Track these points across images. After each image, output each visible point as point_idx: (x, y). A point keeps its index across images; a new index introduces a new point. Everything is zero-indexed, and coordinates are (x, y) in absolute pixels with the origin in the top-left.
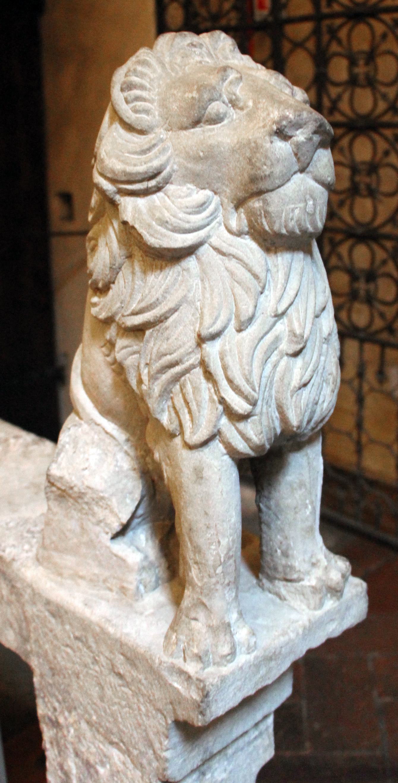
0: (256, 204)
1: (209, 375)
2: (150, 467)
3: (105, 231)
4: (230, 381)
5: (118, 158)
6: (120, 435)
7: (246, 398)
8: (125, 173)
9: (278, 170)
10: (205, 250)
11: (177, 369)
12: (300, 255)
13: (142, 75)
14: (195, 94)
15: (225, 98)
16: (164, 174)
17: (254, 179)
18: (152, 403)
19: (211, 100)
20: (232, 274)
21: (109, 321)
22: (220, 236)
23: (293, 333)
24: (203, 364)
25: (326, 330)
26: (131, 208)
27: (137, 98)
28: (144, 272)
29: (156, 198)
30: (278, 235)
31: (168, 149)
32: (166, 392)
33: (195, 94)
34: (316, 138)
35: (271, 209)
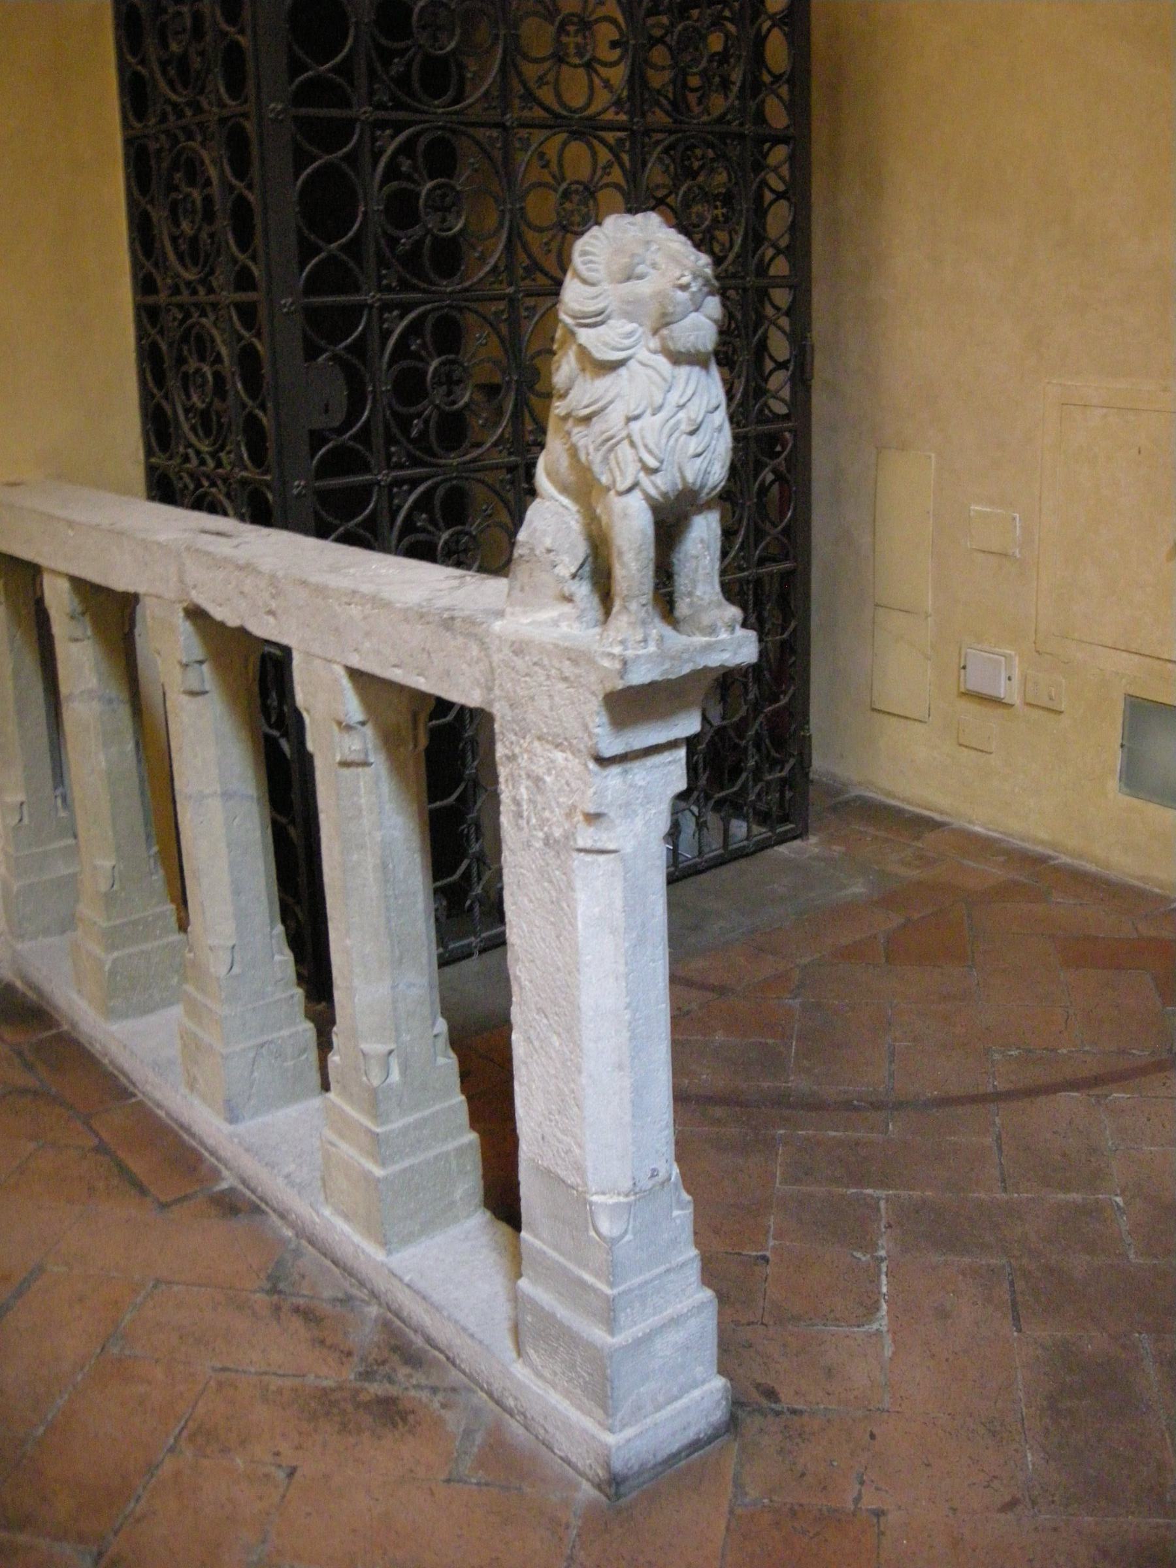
0: (665, 332)
1: (633, 444)
2: (595, 533)
3: (566, 354)
4: (646, 446)
6: (573, 507)
7: (655, 457)
9: (679, 309)
10: (632, 363)
11: (614, 441)
12: (697, 369)
13: (592, 245)
16: (607, 313)
17: (664, 315)
18: (597, 468)
20: (649, 377)
21: (565, 418)
22: (643, 354)
23: (689, 419)
24: (629, 436)
25: (717, 423)
26: (585, 336)
27: (591, 262)
28: (592, 379)
29: (601, 329)
30: (680, 353)
31: (610, 295)
32: (605, 460)
34: (705, 289)
35: (675, 335)
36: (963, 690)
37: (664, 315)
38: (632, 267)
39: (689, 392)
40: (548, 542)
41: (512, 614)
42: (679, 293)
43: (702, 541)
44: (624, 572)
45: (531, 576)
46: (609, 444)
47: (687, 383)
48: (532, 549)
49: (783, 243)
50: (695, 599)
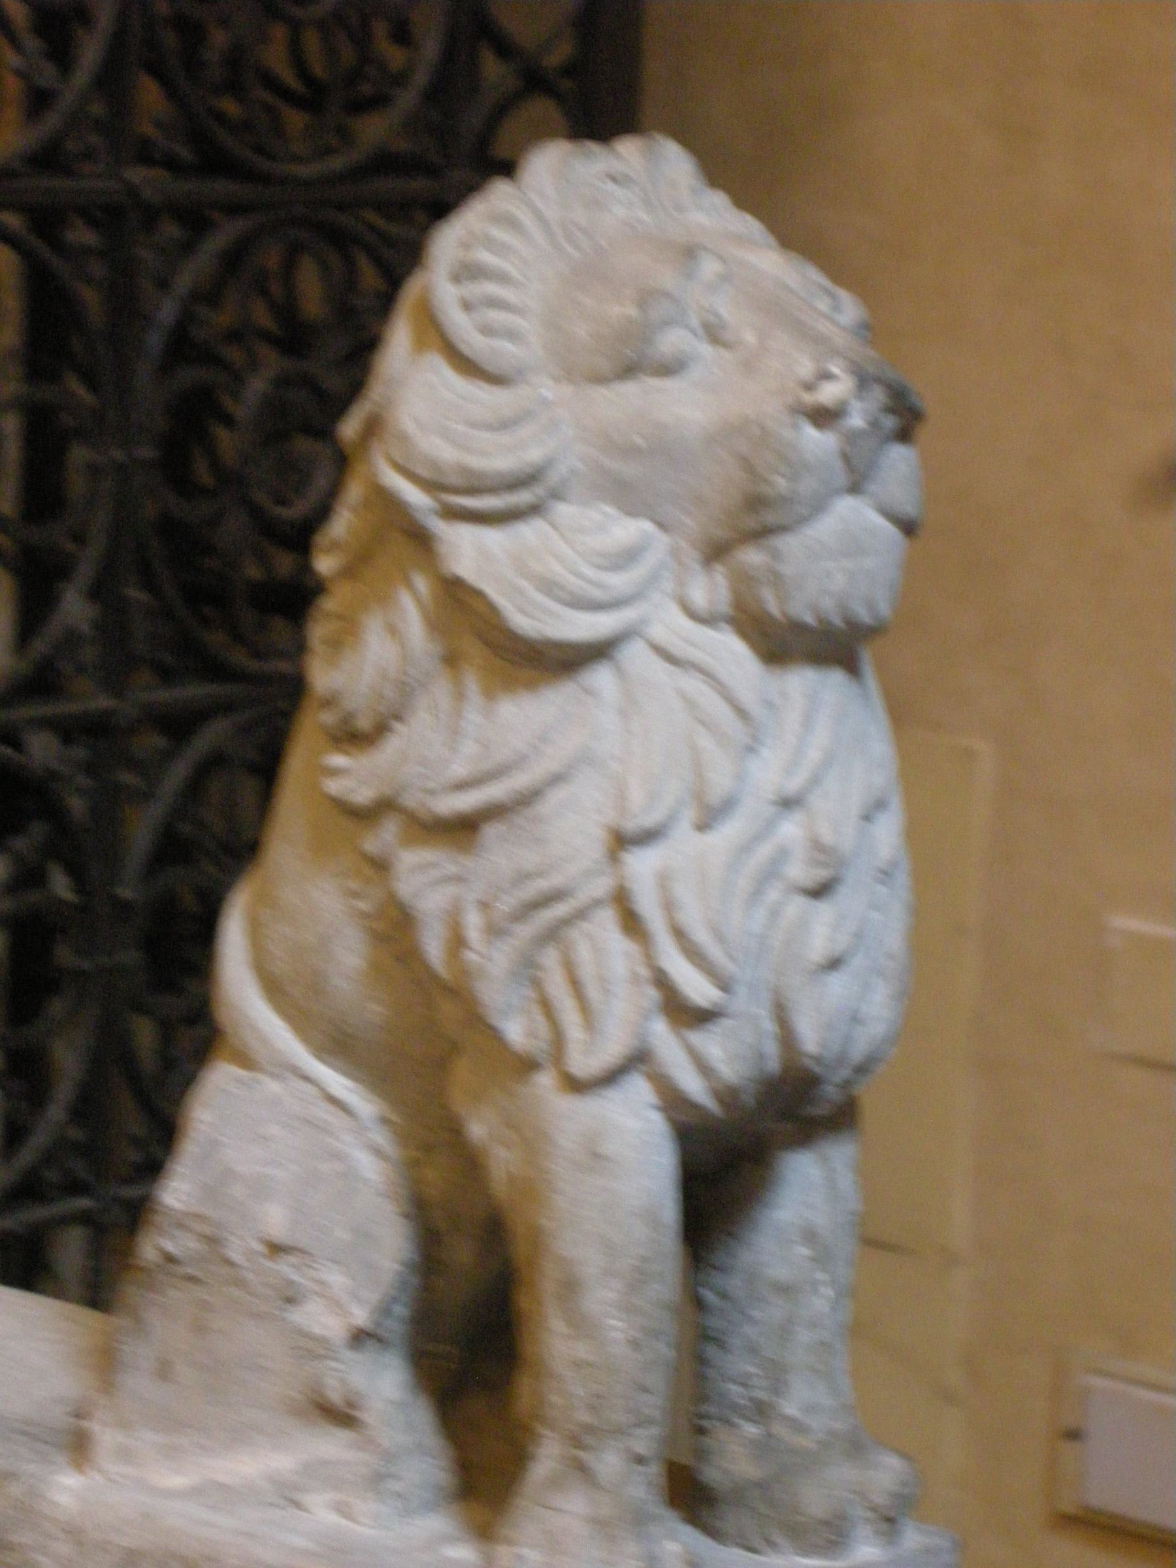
0: (752, 557)
4: (679, 934)
5: (446, 435)
8: (466, 471)
10: (635, 655)
11: (560, 910)
13: (490, 244)
14: (632, 311)
15: (695, 322)
17: (755, 502)
19: (667, 323)
20: (690, 704)
22: (669, 624)
29: (528, 532)
30: (798, 627)
31: (553, 422)
32: (527, 970)
33: (632, 311)
35: (786, 569)
36: (1067, 1506)
37: (755, 502)
38: (644, 332)
39: (814, 755)
40: (276, 1220)
41: (125, 1455)
42: (810, 432)
43: (810, 1236)
44: (582, 1350)
45: (200, 1329)
46: (546, 918)
47: (808, 722)
48: (213, 1241)
49: (560, 54)
50: (778, 1429)
